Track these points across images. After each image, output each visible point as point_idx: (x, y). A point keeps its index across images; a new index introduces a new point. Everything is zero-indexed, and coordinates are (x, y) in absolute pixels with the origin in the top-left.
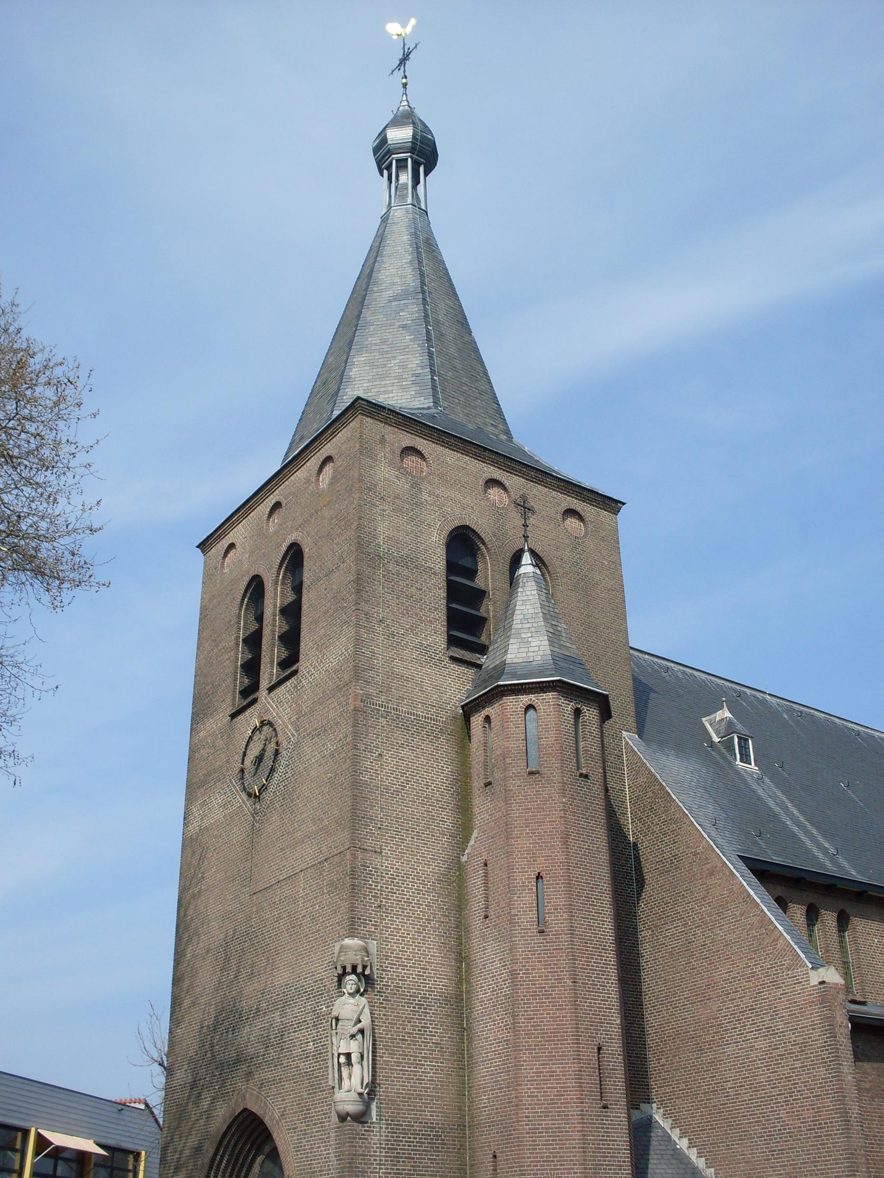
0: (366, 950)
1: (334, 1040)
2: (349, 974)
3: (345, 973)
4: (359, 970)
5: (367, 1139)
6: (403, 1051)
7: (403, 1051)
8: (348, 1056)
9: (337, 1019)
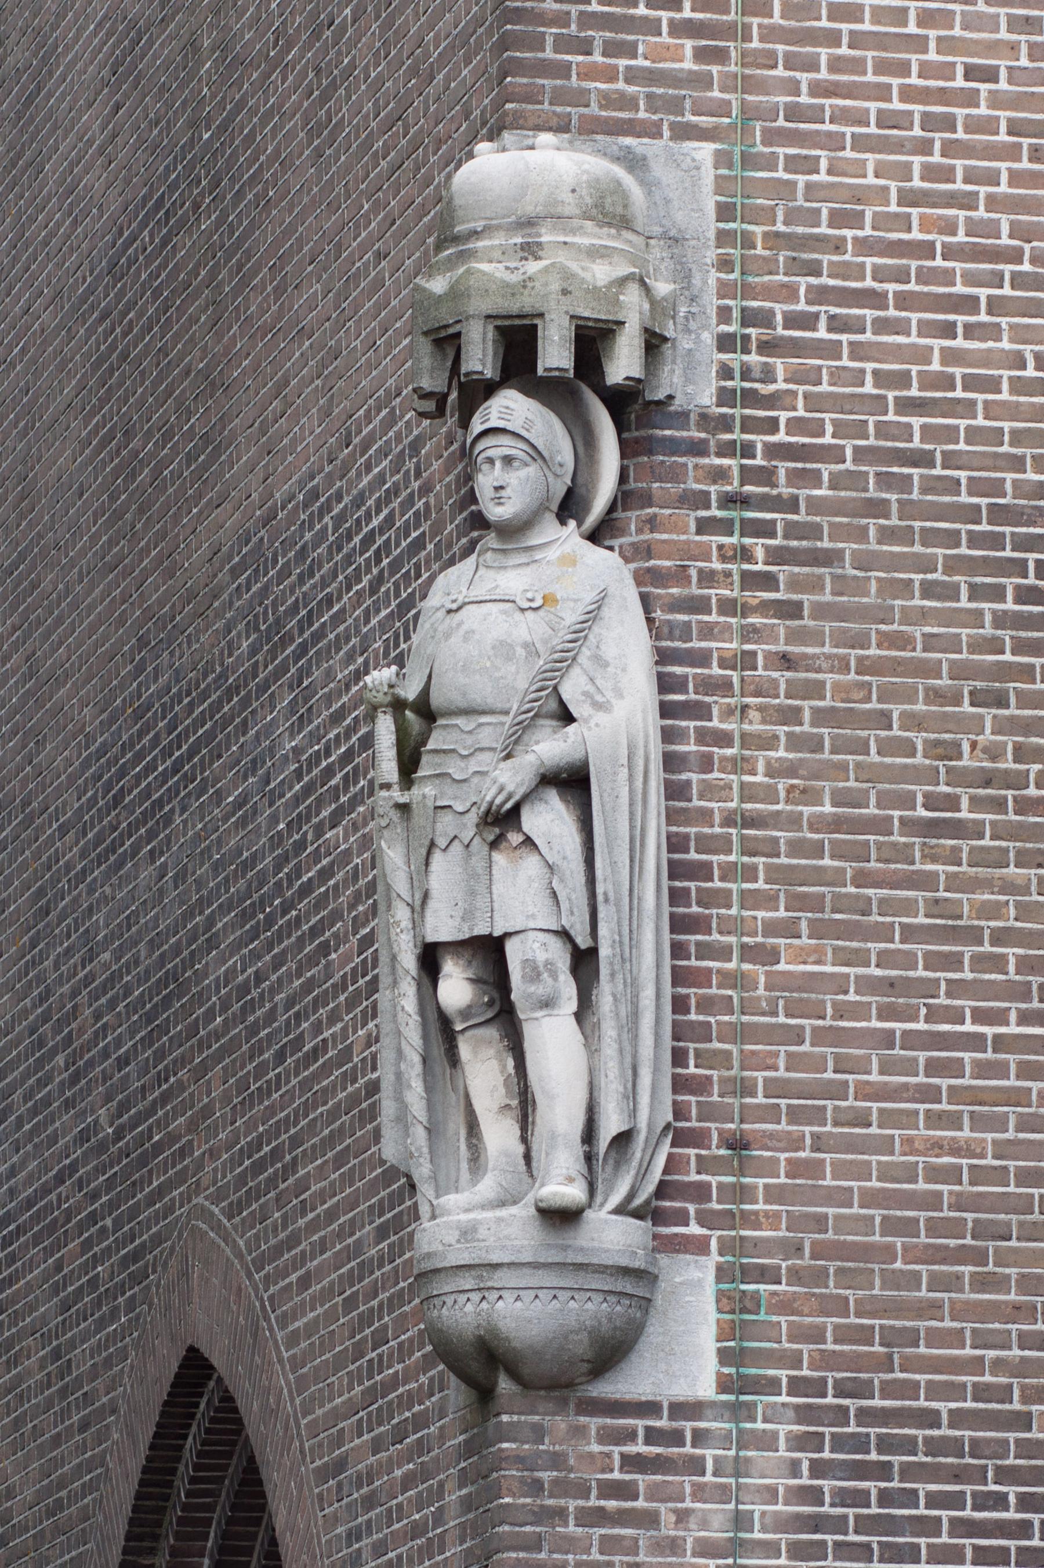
1: (394, 857)
4: (555, 354)
5: (651, 1519)
6: (936, 907)
7: (936, 907)
8: (489, 952)
9: (426, 711)
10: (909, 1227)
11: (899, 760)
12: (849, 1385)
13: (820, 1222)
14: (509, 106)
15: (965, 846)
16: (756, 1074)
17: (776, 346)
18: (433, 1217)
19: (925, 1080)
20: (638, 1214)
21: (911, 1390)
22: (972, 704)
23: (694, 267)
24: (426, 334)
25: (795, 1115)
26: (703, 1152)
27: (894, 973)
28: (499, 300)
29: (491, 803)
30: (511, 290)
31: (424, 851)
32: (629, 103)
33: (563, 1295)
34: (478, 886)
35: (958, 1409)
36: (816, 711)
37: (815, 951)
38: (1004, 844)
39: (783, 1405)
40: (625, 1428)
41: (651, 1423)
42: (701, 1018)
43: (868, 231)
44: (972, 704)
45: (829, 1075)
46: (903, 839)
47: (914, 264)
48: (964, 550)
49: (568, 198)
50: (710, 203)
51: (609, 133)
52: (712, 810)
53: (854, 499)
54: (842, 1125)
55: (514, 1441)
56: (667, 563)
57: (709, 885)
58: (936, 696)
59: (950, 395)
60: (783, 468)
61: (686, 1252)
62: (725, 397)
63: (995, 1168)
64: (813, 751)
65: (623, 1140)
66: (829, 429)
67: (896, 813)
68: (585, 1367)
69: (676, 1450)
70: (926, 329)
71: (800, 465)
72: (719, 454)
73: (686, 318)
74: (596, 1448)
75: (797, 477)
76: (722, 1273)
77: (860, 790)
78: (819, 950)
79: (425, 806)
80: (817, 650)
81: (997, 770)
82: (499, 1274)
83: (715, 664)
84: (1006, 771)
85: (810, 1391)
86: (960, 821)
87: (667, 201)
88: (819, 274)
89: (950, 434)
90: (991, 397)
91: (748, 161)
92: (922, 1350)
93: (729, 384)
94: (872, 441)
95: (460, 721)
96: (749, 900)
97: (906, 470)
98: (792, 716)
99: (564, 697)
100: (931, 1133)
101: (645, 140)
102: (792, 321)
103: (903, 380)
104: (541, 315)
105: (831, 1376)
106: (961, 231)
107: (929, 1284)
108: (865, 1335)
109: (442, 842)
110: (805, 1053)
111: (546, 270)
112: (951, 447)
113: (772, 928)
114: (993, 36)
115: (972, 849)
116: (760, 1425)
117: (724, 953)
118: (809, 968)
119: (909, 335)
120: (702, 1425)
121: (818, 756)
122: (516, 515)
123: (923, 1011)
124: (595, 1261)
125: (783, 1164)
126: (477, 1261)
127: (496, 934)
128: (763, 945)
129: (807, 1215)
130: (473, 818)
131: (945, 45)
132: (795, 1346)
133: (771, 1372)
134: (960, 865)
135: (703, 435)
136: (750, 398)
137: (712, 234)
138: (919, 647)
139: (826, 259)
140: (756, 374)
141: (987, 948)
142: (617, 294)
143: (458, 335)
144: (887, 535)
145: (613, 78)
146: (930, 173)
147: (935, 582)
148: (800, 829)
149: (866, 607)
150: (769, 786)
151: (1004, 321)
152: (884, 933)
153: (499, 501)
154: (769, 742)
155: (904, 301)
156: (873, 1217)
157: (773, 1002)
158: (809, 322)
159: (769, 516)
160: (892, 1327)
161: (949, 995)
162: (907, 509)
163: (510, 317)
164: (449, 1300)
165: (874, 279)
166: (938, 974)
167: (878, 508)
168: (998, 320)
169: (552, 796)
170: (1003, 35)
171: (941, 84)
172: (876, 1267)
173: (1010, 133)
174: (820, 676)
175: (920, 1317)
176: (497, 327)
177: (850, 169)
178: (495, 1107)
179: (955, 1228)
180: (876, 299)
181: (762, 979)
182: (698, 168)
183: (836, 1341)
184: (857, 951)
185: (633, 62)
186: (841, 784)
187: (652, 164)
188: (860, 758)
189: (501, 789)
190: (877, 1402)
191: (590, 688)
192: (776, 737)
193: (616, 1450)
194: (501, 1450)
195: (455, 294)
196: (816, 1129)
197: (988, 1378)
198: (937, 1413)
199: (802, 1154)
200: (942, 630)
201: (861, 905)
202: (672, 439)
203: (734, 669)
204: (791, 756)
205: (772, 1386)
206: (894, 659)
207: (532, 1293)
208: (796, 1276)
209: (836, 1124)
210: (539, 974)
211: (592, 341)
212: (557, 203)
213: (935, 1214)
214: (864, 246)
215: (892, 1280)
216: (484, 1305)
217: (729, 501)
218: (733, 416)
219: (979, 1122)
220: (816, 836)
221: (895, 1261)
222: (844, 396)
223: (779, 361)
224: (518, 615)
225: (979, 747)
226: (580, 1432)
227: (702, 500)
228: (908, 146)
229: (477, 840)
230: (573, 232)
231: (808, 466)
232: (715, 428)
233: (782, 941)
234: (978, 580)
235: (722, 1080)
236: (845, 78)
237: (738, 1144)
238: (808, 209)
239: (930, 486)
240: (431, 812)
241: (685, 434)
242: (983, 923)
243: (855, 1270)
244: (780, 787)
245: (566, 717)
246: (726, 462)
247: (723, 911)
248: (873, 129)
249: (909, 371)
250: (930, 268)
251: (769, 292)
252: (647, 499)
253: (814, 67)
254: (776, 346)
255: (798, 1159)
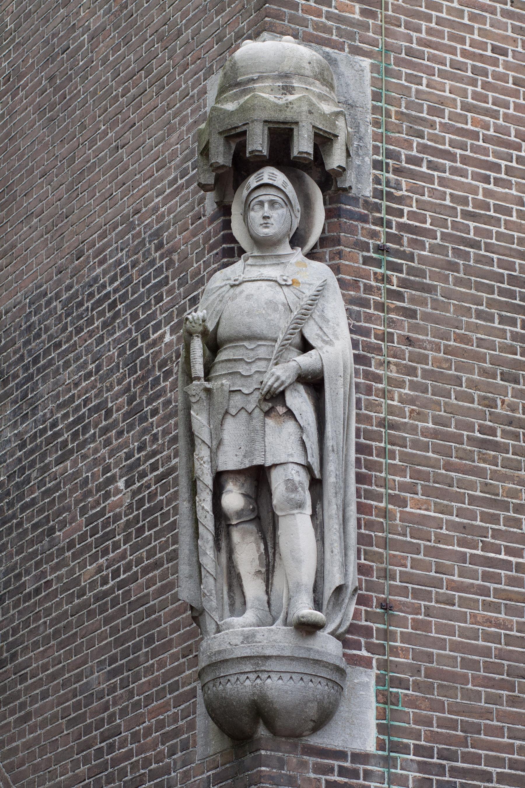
0: (385, 709)
1: (200, 420)
2: (258, 163)
3: (243, 166)
4: (303, 145)
8: (258, 478)
10: (474, 665)
11: (466, 404)
12: (445, 753)
13: (429, 657)
14: (267, 19)
15: (500, 456)
16: (396, 568)
17: (402, 171)
18: (218, 631)
19: (482, 583)
20: (338, 637)
21: (476, 759)
22: (502, 380)
23: (361, 122)
24: (220, 133)
25: (416, 594)
26: (369, 609)
27: (466, 521)
28: (273, 113)
29: (271, 386)
30: (280, 108)
31: (220, 417)
32: (329, 30)
33: (306, 678)
34: (254, 438)
35: (501, 773)
36: (424, 370)
37: (426, 503)
38: (519, 458)
39: (411, 760)
40: (328, 765)
41: (342, 764)
42: (367, 532)
43: (446, 120)
44: (502, 380)
45: (433, 574)
46: (469, 448)
47: (469, 142)
48: (496, 296)
49: (307, 66)
50: (369, 90)
51: (318, 43)
52: (372, 417)
53: (442, 260)
54: (440, 603)
55: (268, 766)
56: (348, 278)
57: (371, 458)
58: (484, 372)
59: (488, 213)
60: (406, 237)
61: (360, 665)
62: (377, 193)
63: (518, 637)
64: (423, 392)
65: (339, 590)
66: (429, 221)
67: (465, 433)
68: (311, 725)
69: (355, 781)
70: (476, 177)
71: (414, 237)
72: (374, 224)
73: (357, 148)
74: (312, 775)
75: (413, 243)
76: (380, 680)
77: (447, 417)
78: (427, 502)
79: (222, 390)
80: (424, 338)
81: (515, 417)
82: (269, 662)
83: (373, 337)
84: (519, 418)
85: (425, 754)
86: (497, 442)
87: (348, 85)
88: (423, 138)
89: (488, 234)
90: (508, 218)
91: (388, 72)
92: (482, 736)
93: (379, 187)
94: (449, 231)
95: (246, 344)
96: (393, 470)
97: (467, 249)
98: (411, 371)
99: (307, 335)
100: (486, 613)
101: (336, 51)
102: (410, 160)
103: (464, 201)
104: (297, 123)
105: (436, 746)
106: (492, 130)
107: (485, 699)
108: (452, 725)
109: (233, 411)
110: (421, 560)
111: (300, 99)
112: (489, 241)
113: (403, 487)
114: (505, 33)
115: (503, 459)
116: (399, 771)
117: (378, 497)
118: (422, 512)
119: (467, 178)
120: (369, 767)
121: (425, 396)
122: (275, 234)
123: (480, 544)
124: (325, 659)
125: (410, 621)
126: (256, 654)
127: (267, 465)
128: (399, 495)
129: (422, 652)
130: (257, 395)
131: (482, 32)
132: (417, 727)
133: (405, 741)
134: (497, 466)
135: (366, 212)
136: (390, 197)
137: (370, 106)
138: (475, 345)
139: (426, 130)
140: (392, 184)
141: (511, 514)
142: (335, 120)
143: (244, 133)
144: (458, 282)
145: (320, 16)
146: (476, 96)
147: (482, 311)
148: (417, 434)
149: (449, 318)
150: (401, 408)
151: (513, 180)
152: (460, 498)
153: (266, 226)
154: (401, 384)
155: (465, 160)
156: (456, 657)
157: (404, 528)
158: (418, 162)
159: (399, 261)
160: (467, 721)
161: (493, 537)
162: (468, 270)
163: (279, 123)
164: (233, 679)
165: (450, 146)
166: (488, 525)
167: (453, 267)
168: (511, 178)
169: (301, 388)
170: (509, 33)
171: (481, 52)
172: (459, 686)
173: (514, 84)
174: (426, 352)
175: (481, 717)
176: (269, 129)
177: (438, 86)
178: (253, 571)
179: (497, 669)
180: (451, 157)
181: (398, 515)
182: (363, 71)
183: (438, 727)
184: (447, 506)
185: (330, 9)
186: (437, 413)
187: (340, 64)
188: (447, 400)
189: (278, 379)
190: (460, 764)
191: (321, 333)
192: (404, 382)
193: (324, 777)
194: (261, 771)
195: (242, 109)
196: (427, 603)
197: (516, 756)
198: (491, 773)
199: (420, 617)
200: (486, 337)
201: (448, 481)
202: (350, 211)
203: (383, 341)
204: (412, 393)
205: (405, 749)
206: (463, 349)
207: (289, 675)
208: (417, 686)
209: (437, 602)
210: (296, 488)
211: (323, 141)
212: (301, 67)
213: (488, 659)
214: (445, 128)
215: (468, 695)
216: (258, 681)
217: (380, 249)
218: (381, 204)
219: (509, 610)
220: (425, 439)
221: (468, 684)
222: (436, 204)
223: (404, 179)
224: (278, 288)
225: (506, 403)
226: (303, 765)
227: (365, 247)
228: (466, 80)
229: (257, 410)
230: (310, 84)
231: (419, 238)
232: (372, 209)
233: (408, 495)
234: (504, 313)
235: (378, 569)
236: (434, 39)
237: (386, 606)
238: (417, 103)
239: (479, 259)
240: (227, 394)
241: (357, 209)
242: (509, 500)
243: (448, 686)
244: (406, 409)
245: (305, 346)
246: (377, 228)
247: (378, 474)
248: (448, 68)
249: (468, 197)
250: (477, 145)
251: (398, 142)
252: (337, 241)
253: (419, 31)
254: (402, 171)
255: (418, 619)
